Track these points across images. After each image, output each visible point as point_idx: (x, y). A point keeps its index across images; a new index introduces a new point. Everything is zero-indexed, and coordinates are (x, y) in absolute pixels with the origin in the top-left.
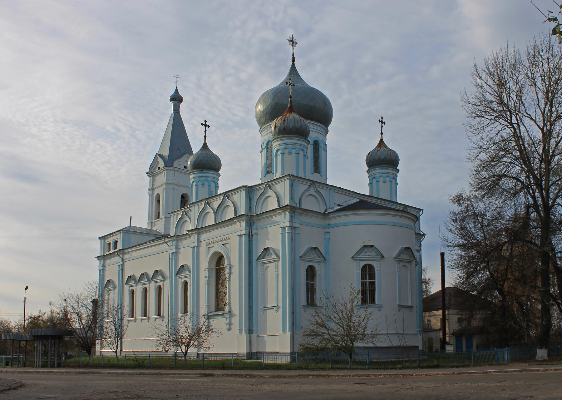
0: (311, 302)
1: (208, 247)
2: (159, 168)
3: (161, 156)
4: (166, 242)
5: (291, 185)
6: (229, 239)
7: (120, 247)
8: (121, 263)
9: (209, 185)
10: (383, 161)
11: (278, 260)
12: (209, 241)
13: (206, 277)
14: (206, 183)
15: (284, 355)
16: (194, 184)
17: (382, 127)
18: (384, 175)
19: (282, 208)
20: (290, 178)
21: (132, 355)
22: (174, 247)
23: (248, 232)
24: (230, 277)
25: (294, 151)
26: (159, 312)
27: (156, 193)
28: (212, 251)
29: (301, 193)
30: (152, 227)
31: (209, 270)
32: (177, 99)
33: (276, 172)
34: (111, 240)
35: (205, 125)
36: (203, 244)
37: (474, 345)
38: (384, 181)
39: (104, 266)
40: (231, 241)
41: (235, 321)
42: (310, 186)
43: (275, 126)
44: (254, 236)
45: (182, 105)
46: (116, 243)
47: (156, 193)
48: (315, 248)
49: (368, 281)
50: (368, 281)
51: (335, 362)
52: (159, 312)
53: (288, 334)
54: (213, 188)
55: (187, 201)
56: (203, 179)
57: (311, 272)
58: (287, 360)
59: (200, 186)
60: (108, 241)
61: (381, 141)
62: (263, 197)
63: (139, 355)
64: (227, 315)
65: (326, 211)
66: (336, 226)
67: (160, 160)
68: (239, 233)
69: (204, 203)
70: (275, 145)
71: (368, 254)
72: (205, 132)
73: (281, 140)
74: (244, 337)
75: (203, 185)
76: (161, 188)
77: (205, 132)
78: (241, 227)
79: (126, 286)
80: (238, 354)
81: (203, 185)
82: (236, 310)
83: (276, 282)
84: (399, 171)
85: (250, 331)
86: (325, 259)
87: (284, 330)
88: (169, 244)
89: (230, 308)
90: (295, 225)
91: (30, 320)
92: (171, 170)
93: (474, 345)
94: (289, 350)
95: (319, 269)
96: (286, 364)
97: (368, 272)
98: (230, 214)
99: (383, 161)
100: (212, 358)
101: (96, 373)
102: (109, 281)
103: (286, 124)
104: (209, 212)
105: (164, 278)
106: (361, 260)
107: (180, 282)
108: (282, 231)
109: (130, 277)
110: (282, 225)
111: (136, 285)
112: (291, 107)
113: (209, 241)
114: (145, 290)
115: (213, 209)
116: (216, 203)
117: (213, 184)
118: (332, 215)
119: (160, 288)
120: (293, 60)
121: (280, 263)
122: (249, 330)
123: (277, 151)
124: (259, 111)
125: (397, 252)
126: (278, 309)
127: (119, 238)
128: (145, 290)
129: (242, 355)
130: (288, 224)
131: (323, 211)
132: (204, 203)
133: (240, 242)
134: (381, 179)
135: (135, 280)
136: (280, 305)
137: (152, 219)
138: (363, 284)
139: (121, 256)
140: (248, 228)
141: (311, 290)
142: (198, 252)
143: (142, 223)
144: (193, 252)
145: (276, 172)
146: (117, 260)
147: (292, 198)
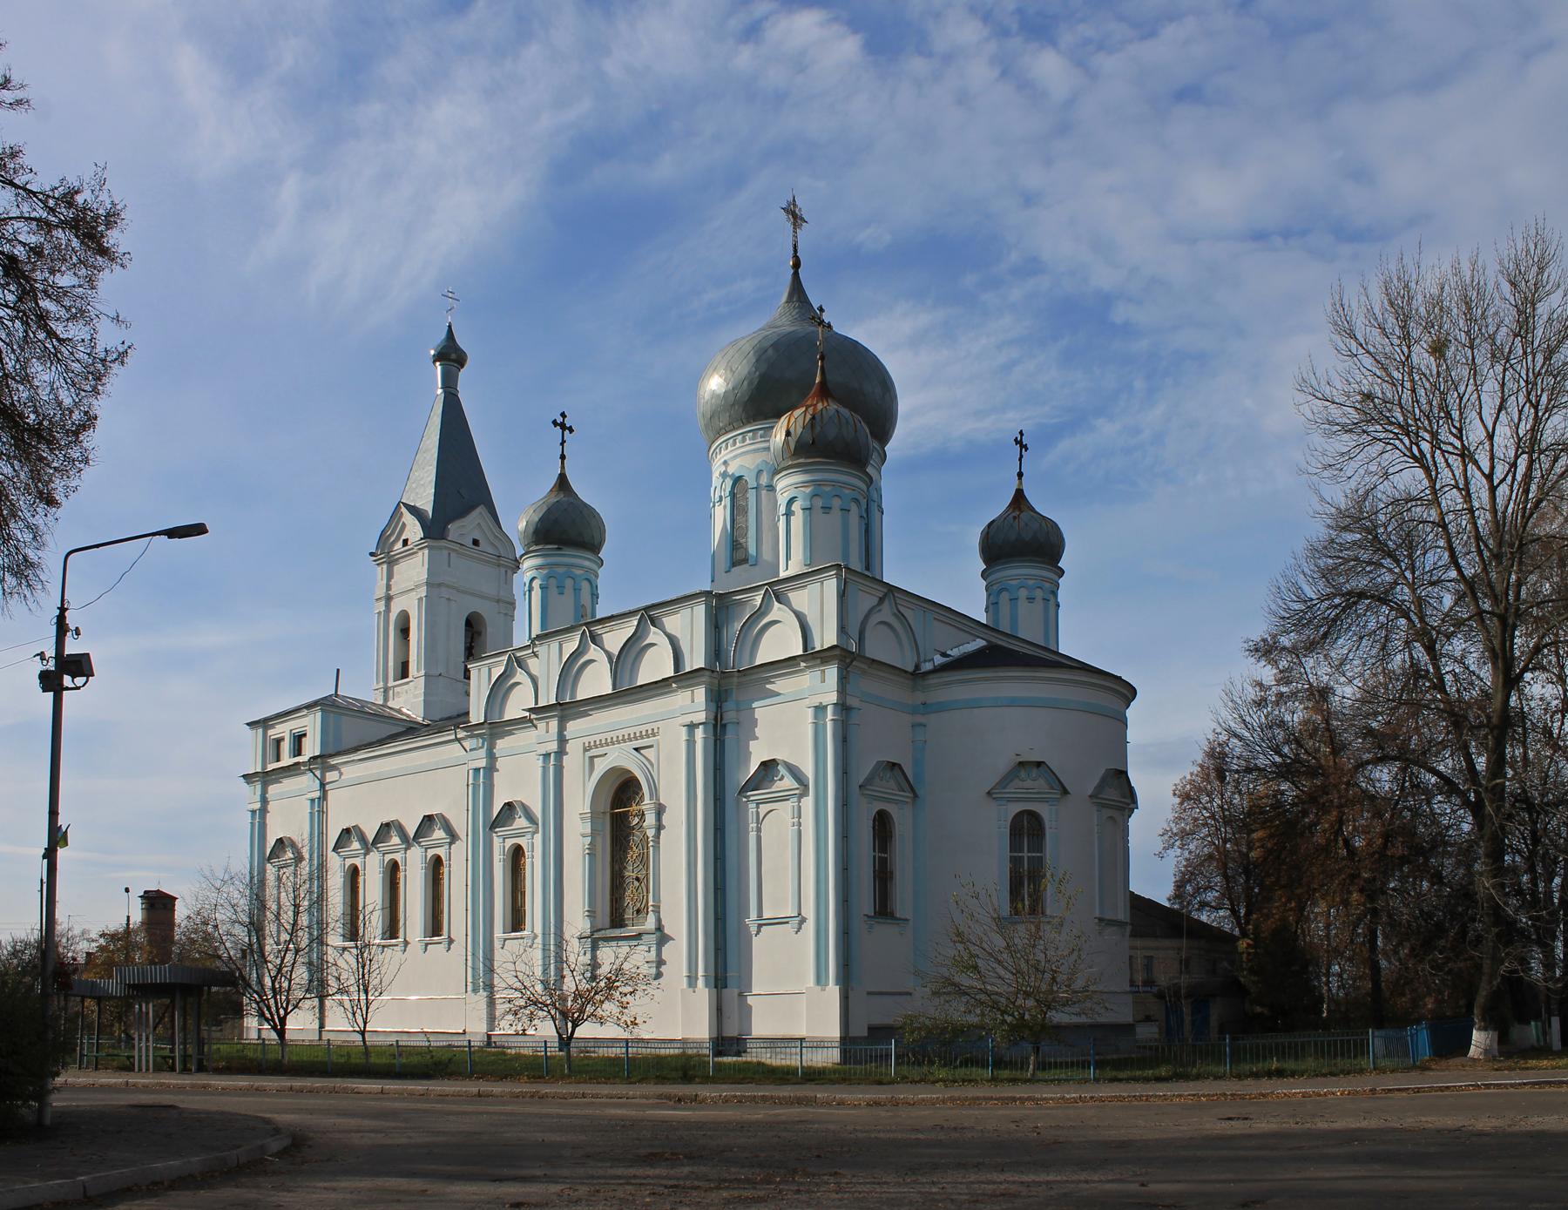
0: (884, 909)
1: (589, 754)
2: (405, 542)
3: (414, 510)
4: (458, 740)
5: (842, 595)
6: (654, 735)
7: (311, 748)
8: (317, 794)
9: (577, 590)
10: (1023, 545)
11: (805, 793)
12: (592, 739)
13: (584, 836)
14: (569, 583)
15: (819, 1044)
16: (536, 584)
17: (563, 442)
18: (1031, 582)
19: (813, 657)
20: (838, 576)
21: (420, 1042)
22: (483, 753)
23: (712, 716)
24: (657, 836)
25: (836, 503)
26: (435, 926)
27: (396, 609)
28: (601, 767)
29: (861, 617)
30: (386, 699)
31: (595, 815)
32: (451, 356)
33: (788, 558)
34: (283, 730)
35: (563, 426)
36: (573, 747)
37: (1214, 1021)
38: (1031, 599)
39: (264, 801)
40: (665, 741)
41: (676, 953)
42: (881, 600)
43: (788, 434)
44: (729, 728)
45: (464, 375)
46: (298, 739)
47: (396, 609)
48: (894, 764)
49: (1026, 854)
50: (1026, 854)
51: (999, 1063)
52: (435, 926)
53: (833, 991)
54: (586, 598)
55: (479, 634)
56: (561, 570)
57: (882, 824)
58: (832, 1057)
59: (554, 591)
60: (273, 733)
61: (1019, 496)
62: (756, 624)
63: (405, 1041)
64: (652, 939)
65: (917, 667)
66: (942, 708)
67: (408, 518)
68: (688, 719)
69: (577, 637)
70: (788, 485)
71: (1029, 783)
72: (562, 444)
73: (806, 472)
74: (703, 995)
75: (561, 588)
76: (415, 596)
77: (562, 444)
78: (693, 703)
79: (331, 855)
80: (684, 1041)
81: (561, 588)
82: (676, 925)
83: (793, 854)
84: (1061, 572)
85: (719, 981)
86: (916, 796)
87: (820, 979)
88: (467, 744)
89: (659, 920)
90: (851, 701)
91: (102, 941)
92: (440, 548)
93: (1214, 1021)
94: (834, 1032)
95: (902, 819)
96: (824, 1068)
97: (1027, 829)
98: (656, 665)
99: (1023, 545)
100: (602, 1052)
101: (345, 1090)
102: (280, 841)
103: (818, 429)
104: (592, 661)
105: (453, 837)
106: (1010, 800)
107: (500, 847)
108: (816, 717)
109: (347, 832)
110: (816, 701)
111: (365, 855)
112: (823, 382)
113: (592, 739)
114: (393, 870)
115: (607, 652)
116: (615, 639)
117: (585, 586)
118: (934, 680)
119: (437, 862)
120: (797, 265)
121: (808, 803)
122: (716, 979)
123: (791, 501)
124: (714, 395)
125: (1096, 782)
126: (803, 920)
127: (311, 724)
128: (393, 870)
129: (700, 1043)
130: (833, 697)
131: (910, 669)
132: (577, 637)
133: (691, 743)
134: (1023, 593)
135: (362, 838)
136: (809, 911)
137: (386, 680)
138: (1012, 859)
139: (318, 773)
140: (713, 706)
141: (883, 876)
142: (559, 769)
143: (363, 688)
144: (545, 769)
145: (788, 558)
146: (306, 784)
147: (842, 629)
